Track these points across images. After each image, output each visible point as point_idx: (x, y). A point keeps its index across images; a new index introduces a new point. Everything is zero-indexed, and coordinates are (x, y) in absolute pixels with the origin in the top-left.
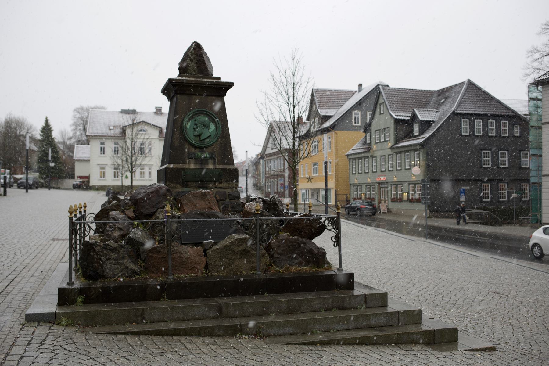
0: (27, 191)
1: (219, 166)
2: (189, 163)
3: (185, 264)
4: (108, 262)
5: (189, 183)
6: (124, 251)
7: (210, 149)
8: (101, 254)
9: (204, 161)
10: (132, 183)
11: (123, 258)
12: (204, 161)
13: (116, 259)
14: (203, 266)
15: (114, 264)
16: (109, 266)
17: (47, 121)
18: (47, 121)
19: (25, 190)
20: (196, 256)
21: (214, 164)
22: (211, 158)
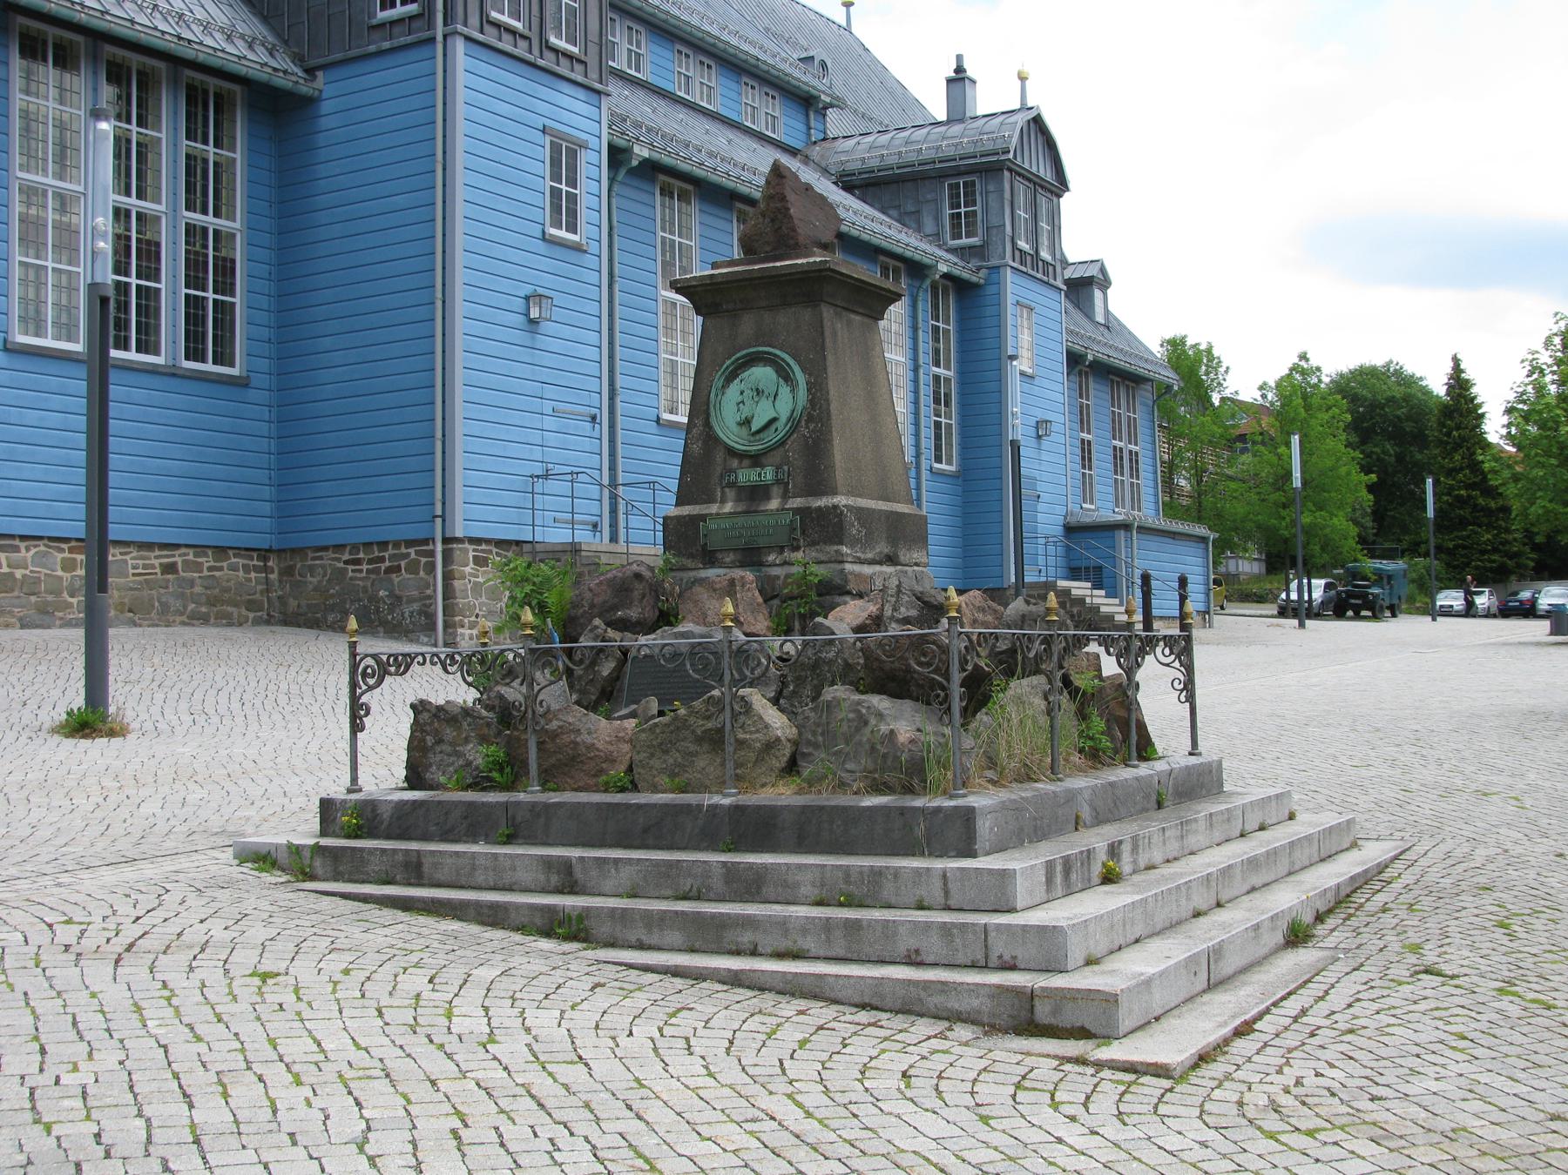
0: (1302, 625)
1: (796, 503)
2: (723, 501)
3: (582, 762)
4: (438, 749)
5: (719, 556)
6: (469, 725)
7: (777, 457)
8: (428, 728)
9: (755, 494)
10: (117, 543)
11: (467, 740)
12: (755, 494)
13: (453, 744)
14: (623, 767)
15: (449, 755)
16: (438, 758)
17: (1456, 361)
18: (1456, 361)
19: (1295, 622)
20: (610, 743)
21: (785, 496)
22: (778, 482)
